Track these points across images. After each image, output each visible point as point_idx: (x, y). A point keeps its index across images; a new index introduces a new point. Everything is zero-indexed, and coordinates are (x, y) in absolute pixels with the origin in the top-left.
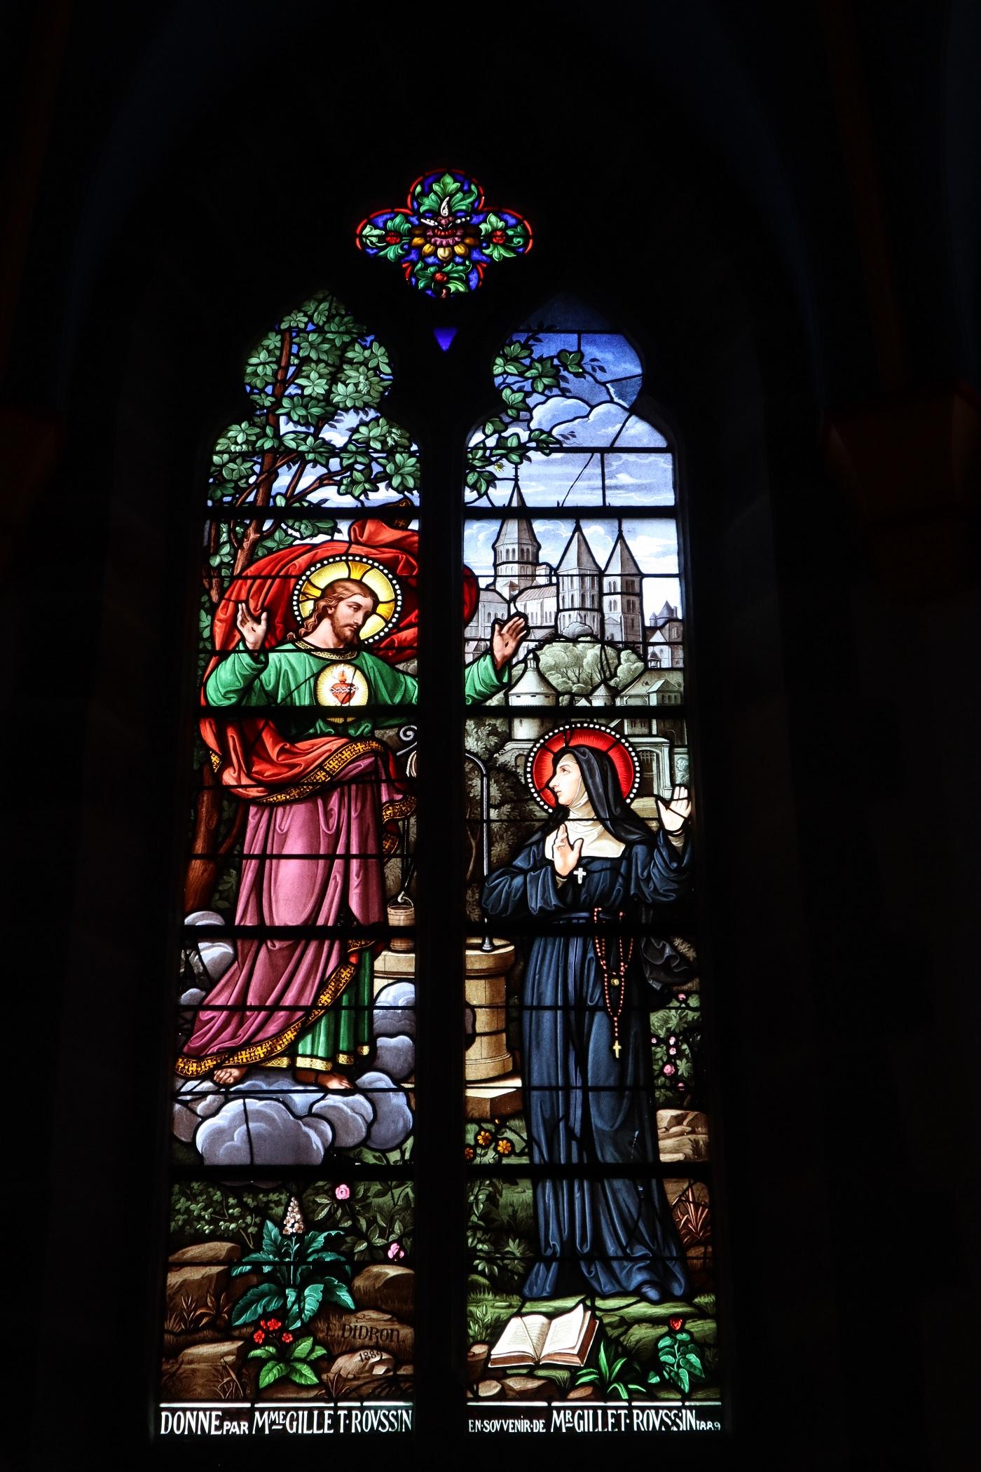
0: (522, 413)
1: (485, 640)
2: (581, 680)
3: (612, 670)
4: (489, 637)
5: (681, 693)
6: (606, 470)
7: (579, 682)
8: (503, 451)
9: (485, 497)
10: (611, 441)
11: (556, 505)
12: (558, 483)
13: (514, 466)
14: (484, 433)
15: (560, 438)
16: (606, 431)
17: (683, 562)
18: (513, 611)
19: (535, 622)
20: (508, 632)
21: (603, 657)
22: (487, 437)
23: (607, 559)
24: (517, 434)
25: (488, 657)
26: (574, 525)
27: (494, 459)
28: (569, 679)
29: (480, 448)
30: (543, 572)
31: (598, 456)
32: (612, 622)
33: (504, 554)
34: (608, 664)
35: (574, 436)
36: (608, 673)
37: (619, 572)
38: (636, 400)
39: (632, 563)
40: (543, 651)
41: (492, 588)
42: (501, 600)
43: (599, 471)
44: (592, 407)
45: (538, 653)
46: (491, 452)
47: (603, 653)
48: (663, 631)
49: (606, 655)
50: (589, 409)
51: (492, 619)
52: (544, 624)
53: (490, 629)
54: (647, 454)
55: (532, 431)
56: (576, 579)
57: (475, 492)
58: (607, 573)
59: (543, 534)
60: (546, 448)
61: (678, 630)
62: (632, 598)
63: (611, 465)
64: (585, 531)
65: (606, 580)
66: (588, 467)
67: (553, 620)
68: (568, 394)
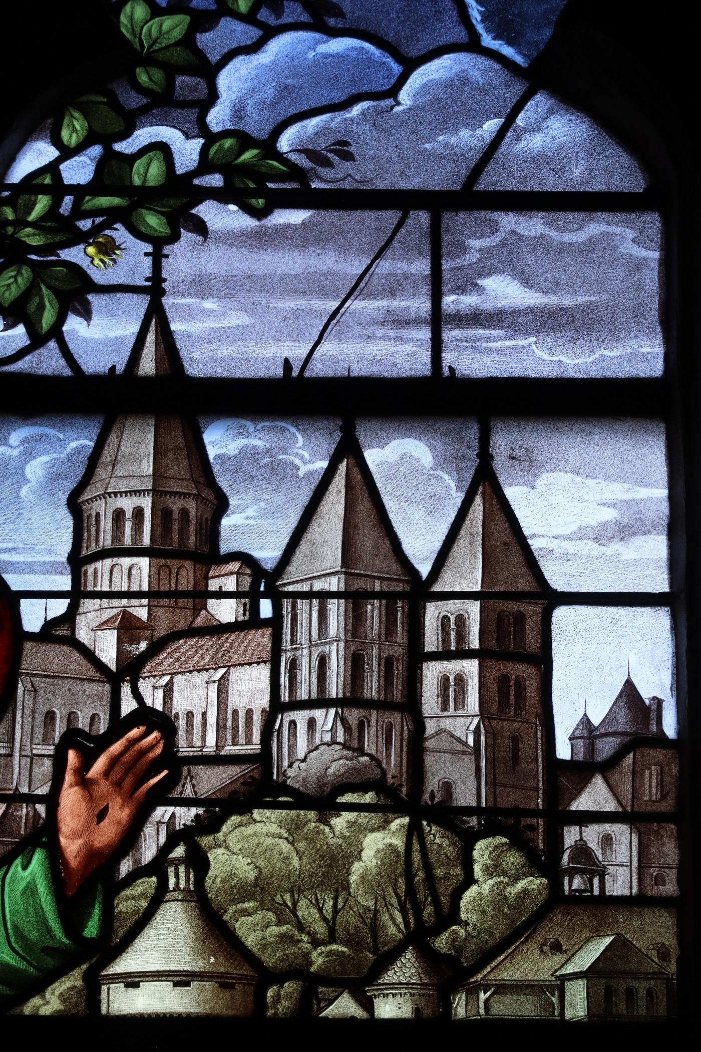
1: (32, 799)
2: (340, 932)
3: (445, 900)
5: (668, 980)
7: (332, 937)
8: (116, 201)
9: (52, 344)
10: (464, 173)
11: (279, 373)
13: (149, 248)
14: (57, 142)
15: (302, 161)
16: (453, 140)
17: (682, 555)
18: (128, 705)
19: (197, 742)
20: (107, 773)
21: (416, 857)
22: (67, 153)
23: (438, 545)
24: (163, 149)
26: (338, 436)
27: (85, 225)
28: (301, 927)
30: (230, 584)
31: (421, 218)
32: (446, 744)
33: (107, 525)
34: (430, 879)
35: (348, 156)
36: (429, 910)
37: (477, 587)
38: (550, 43)
39: (517, 559)
40: (220, 836)
42: (89, 670)
43: (421, 266)
44: (410, 65)
45: (205, 841)
46: (76, 205)
47: (416, 846)
48: (615, 777)
49: (424, 851)
51: (60, 728)
52: (229, 749)
54: (580, 216)
55: (211, 138)
56: (335, 608)
57: (20, 329)
58: (437, 588)
59: (235, 463)
60: (256, 194)
61: (661, 774)
62: (515, 670)
63: (463, 249)
64: (373, 456)
65: (433, 612)
66: (389, 253)
67: (256, 736)
68: (332, 22)
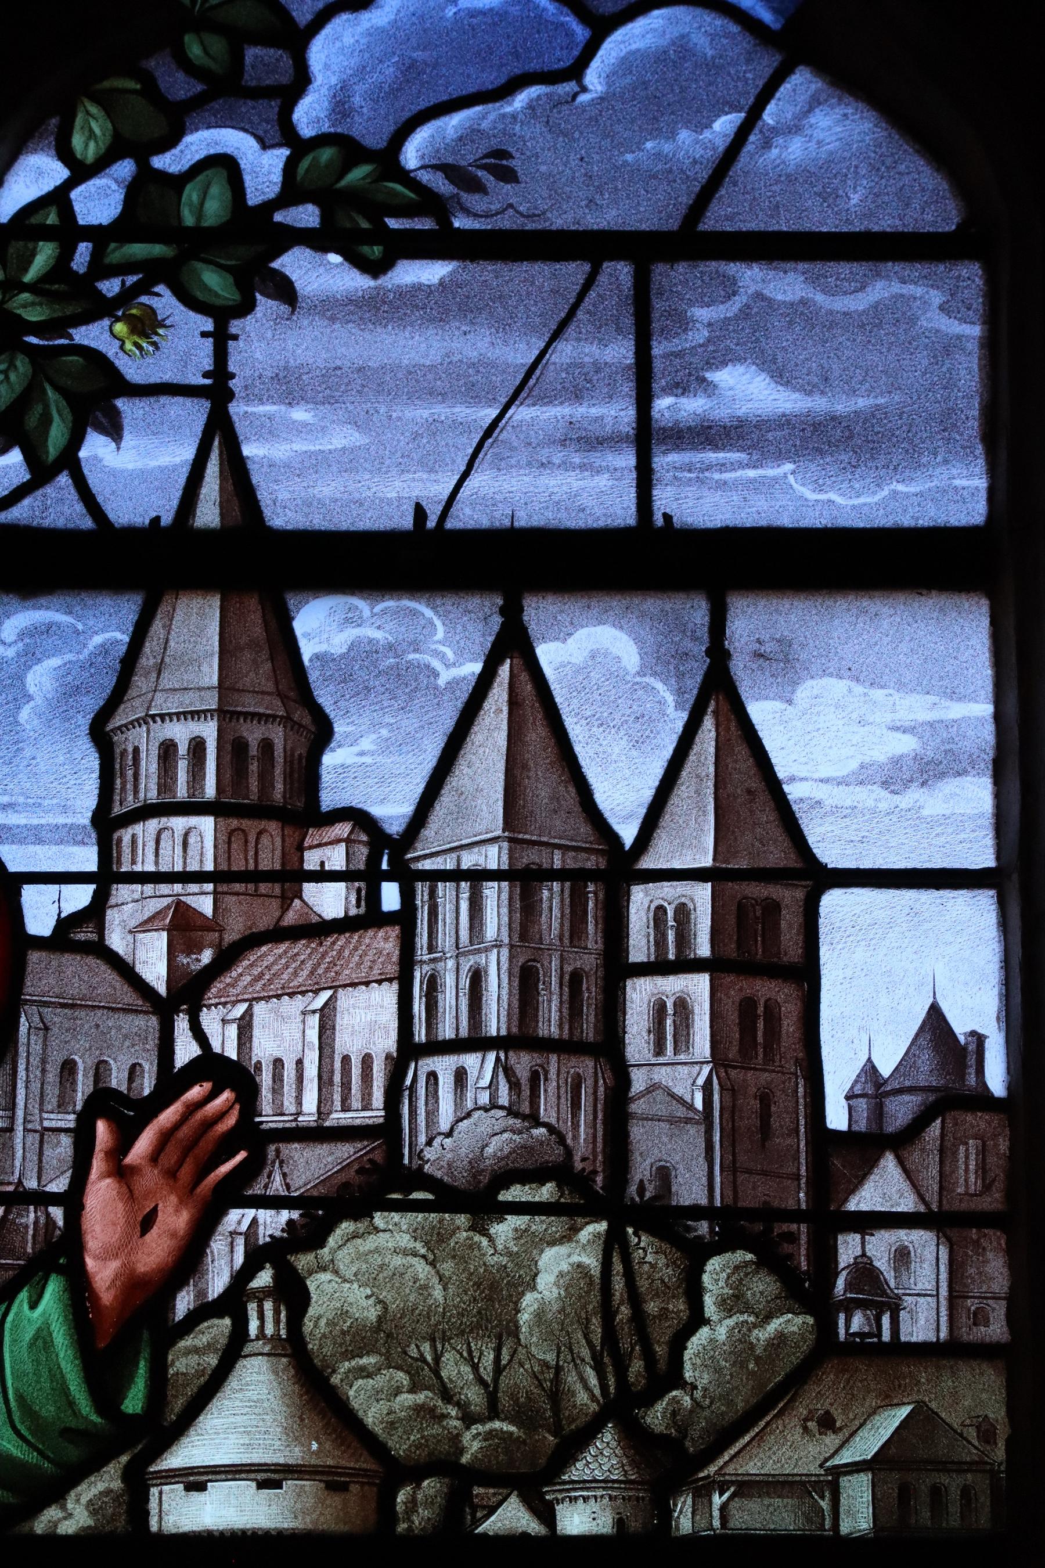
0: (252, 53)
2: (504, 1401)
4: (59, 1185)
5: (993, 1474)
6: (658, 349)
7: (493, 1411)
8: (157, 250)
9: (64, 479)
11: (407, 522)
12: (422, 412)
13: (209, 325)
14: (65, 155)
16: (667, 147)
18: (186, 1051)
19: (290, 1107)
20: (155, 1156)
21: (618, 1284)
23: (648, 794)
25: (53, 1289)
26: (497, 621)
27: (110, 287)
28: (447, 1395)
29: (46, 233)
30: (336, 859)
32: (661, 1106)
33: (150, 765)
34: (639, 1316)
35: (508, 176)
36: (637, 1366)
37: (706, 861)
39: (767, 815)
41: (84, 935)
42: (128, 996)
45: (303, 1261)
46: (96, 256)
47: (618, 1267)
48: (914, 1157)
50: (581, 33)
51: (83, 1087)
52: (338, 1118)
53: (66, 1141)
56: (493, 893)
58: (648, 862)
61: (983, 1152)
62: (765, 989)
63: (684, 323)
64: (547, 654)
66: (571, 331)
